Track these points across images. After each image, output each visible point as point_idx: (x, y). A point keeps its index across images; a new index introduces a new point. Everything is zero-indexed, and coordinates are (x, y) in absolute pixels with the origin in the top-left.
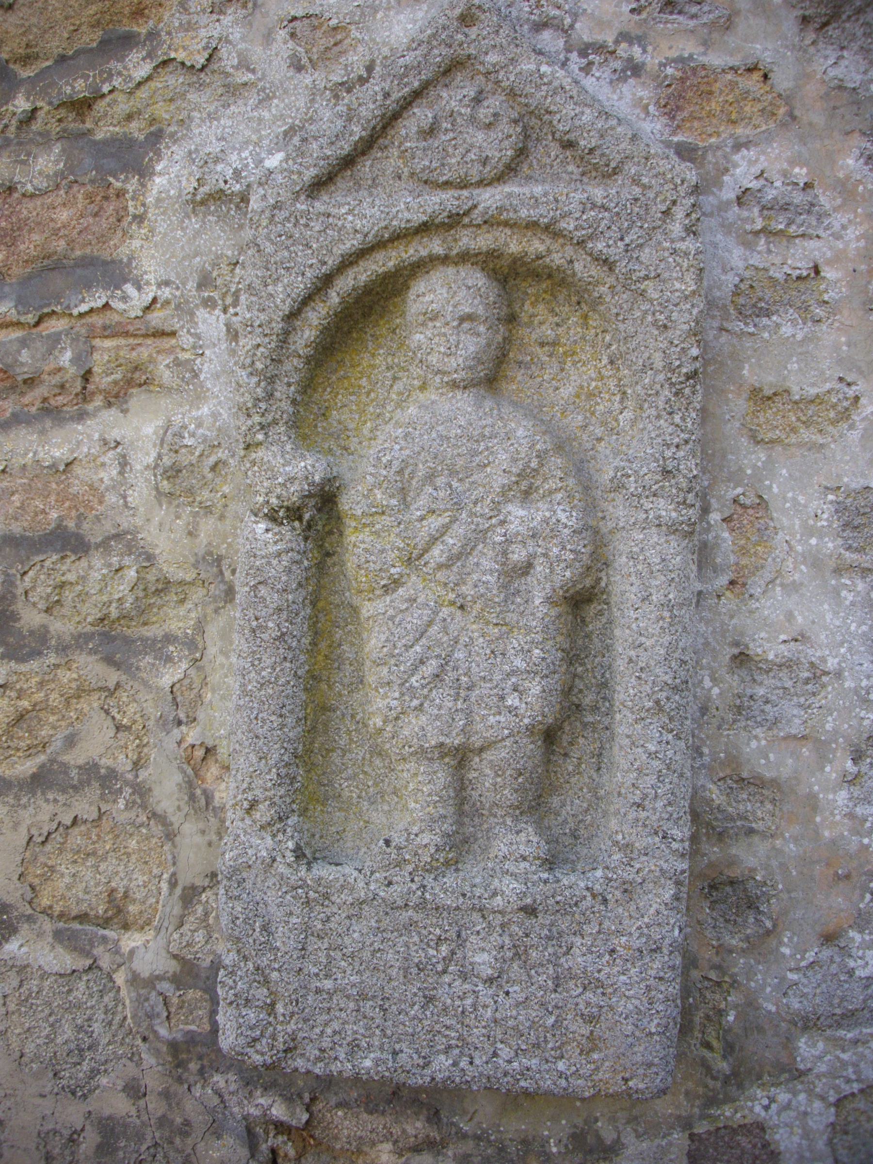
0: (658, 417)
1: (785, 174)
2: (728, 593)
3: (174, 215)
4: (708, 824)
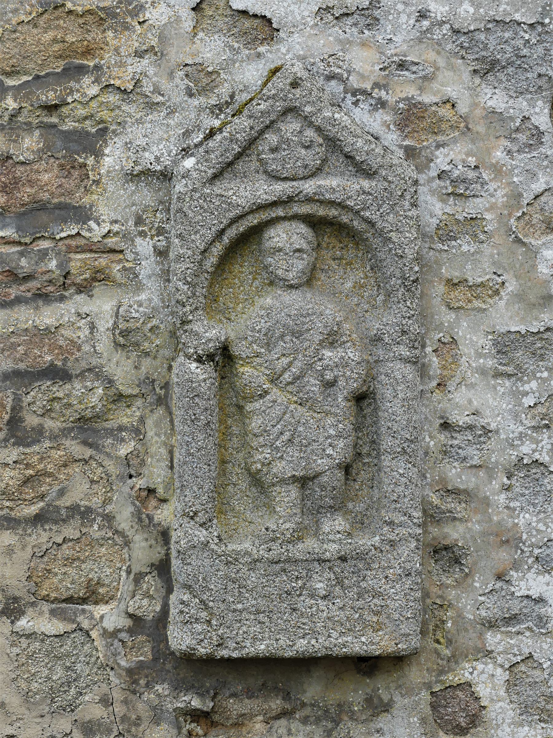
0: (399, 302)
1: (464, 161)
2: (437, 391)
3: (118, 181)
4: (432, 516)
